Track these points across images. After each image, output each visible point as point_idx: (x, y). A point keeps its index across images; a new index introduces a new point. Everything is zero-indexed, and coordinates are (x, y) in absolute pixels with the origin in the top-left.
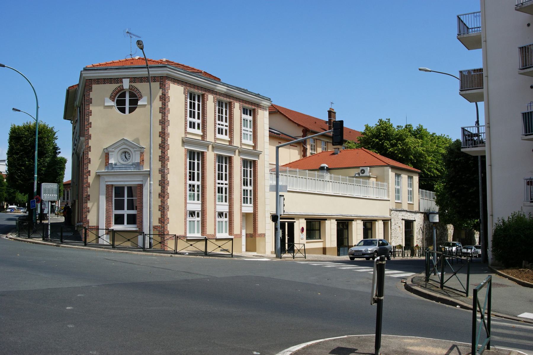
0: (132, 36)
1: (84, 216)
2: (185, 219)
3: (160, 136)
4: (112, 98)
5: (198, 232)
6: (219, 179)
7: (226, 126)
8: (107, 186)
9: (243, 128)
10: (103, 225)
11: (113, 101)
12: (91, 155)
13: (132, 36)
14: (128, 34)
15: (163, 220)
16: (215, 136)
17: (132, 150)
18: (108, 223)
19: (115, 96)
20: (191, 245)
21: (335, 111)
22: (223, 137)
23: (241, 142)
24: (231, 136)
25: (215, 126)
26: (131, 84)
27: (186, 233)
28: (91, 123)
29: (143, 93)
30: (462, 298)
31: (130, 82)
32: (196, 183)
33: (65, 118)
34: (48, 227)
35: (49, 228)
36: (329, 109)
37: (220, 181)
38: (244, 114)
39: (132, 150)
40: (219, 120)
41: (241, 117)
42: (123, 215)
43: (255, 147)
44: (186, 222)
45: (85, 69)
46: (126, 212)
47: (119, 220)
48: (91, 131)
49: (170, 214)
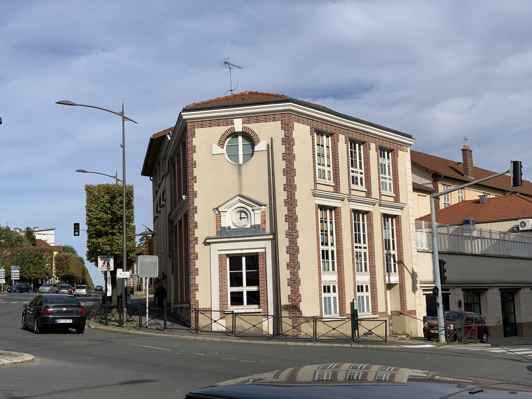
0: (231, 67)
1: (192, 296)
2: (320, 295)
3: (285, 190)
4: (221, 144)
5: (335, 312)
6: (356, 242)
7: (361, 173)
8: (221, 257)
9: (381, 175)
10: (216, 306)
11: (223, 148)
12: (198, 218)
13: (231, 67)
14: (227, 65)
15: (295, 296)
16: (350, 187)
17: (250, 209)
18: (223, 302)
19: (224, 142)
20: (334, 329)
21: (470, 149)
22: (359, 187)
23: (380, 193)
24: (369, 186)
25: (349, 173)
26: (244, 125)
27: (321, 313)
28: (196, 177)
29: (260, 136)
30: (231, 337)
31: (243, 123)
32: (329, 248)
33: (144, 173)
34: (146, 310)
35: (147, 312)
36: (463, 147)
37: (358, 245)
38: (381, 157)
39: (250, 209)
40: (352, 166)
41: (378, 161)
42: (242, 293)
43: (397, 199)
44: (320, 299)
45: (185, 110)
46: (245, 289)
47: (237, 299)
48: (197, 187)
49: (303, 290)
